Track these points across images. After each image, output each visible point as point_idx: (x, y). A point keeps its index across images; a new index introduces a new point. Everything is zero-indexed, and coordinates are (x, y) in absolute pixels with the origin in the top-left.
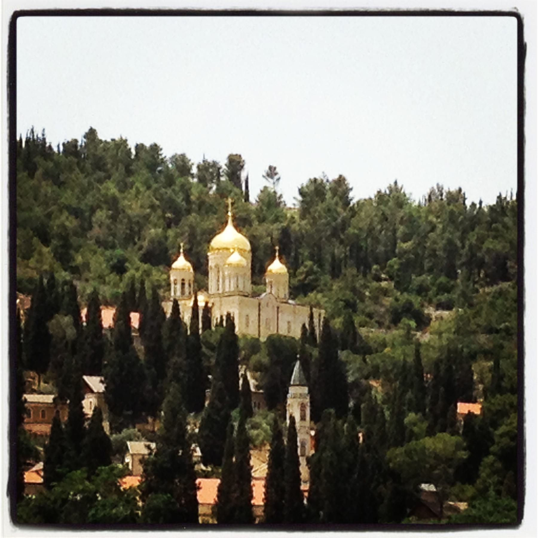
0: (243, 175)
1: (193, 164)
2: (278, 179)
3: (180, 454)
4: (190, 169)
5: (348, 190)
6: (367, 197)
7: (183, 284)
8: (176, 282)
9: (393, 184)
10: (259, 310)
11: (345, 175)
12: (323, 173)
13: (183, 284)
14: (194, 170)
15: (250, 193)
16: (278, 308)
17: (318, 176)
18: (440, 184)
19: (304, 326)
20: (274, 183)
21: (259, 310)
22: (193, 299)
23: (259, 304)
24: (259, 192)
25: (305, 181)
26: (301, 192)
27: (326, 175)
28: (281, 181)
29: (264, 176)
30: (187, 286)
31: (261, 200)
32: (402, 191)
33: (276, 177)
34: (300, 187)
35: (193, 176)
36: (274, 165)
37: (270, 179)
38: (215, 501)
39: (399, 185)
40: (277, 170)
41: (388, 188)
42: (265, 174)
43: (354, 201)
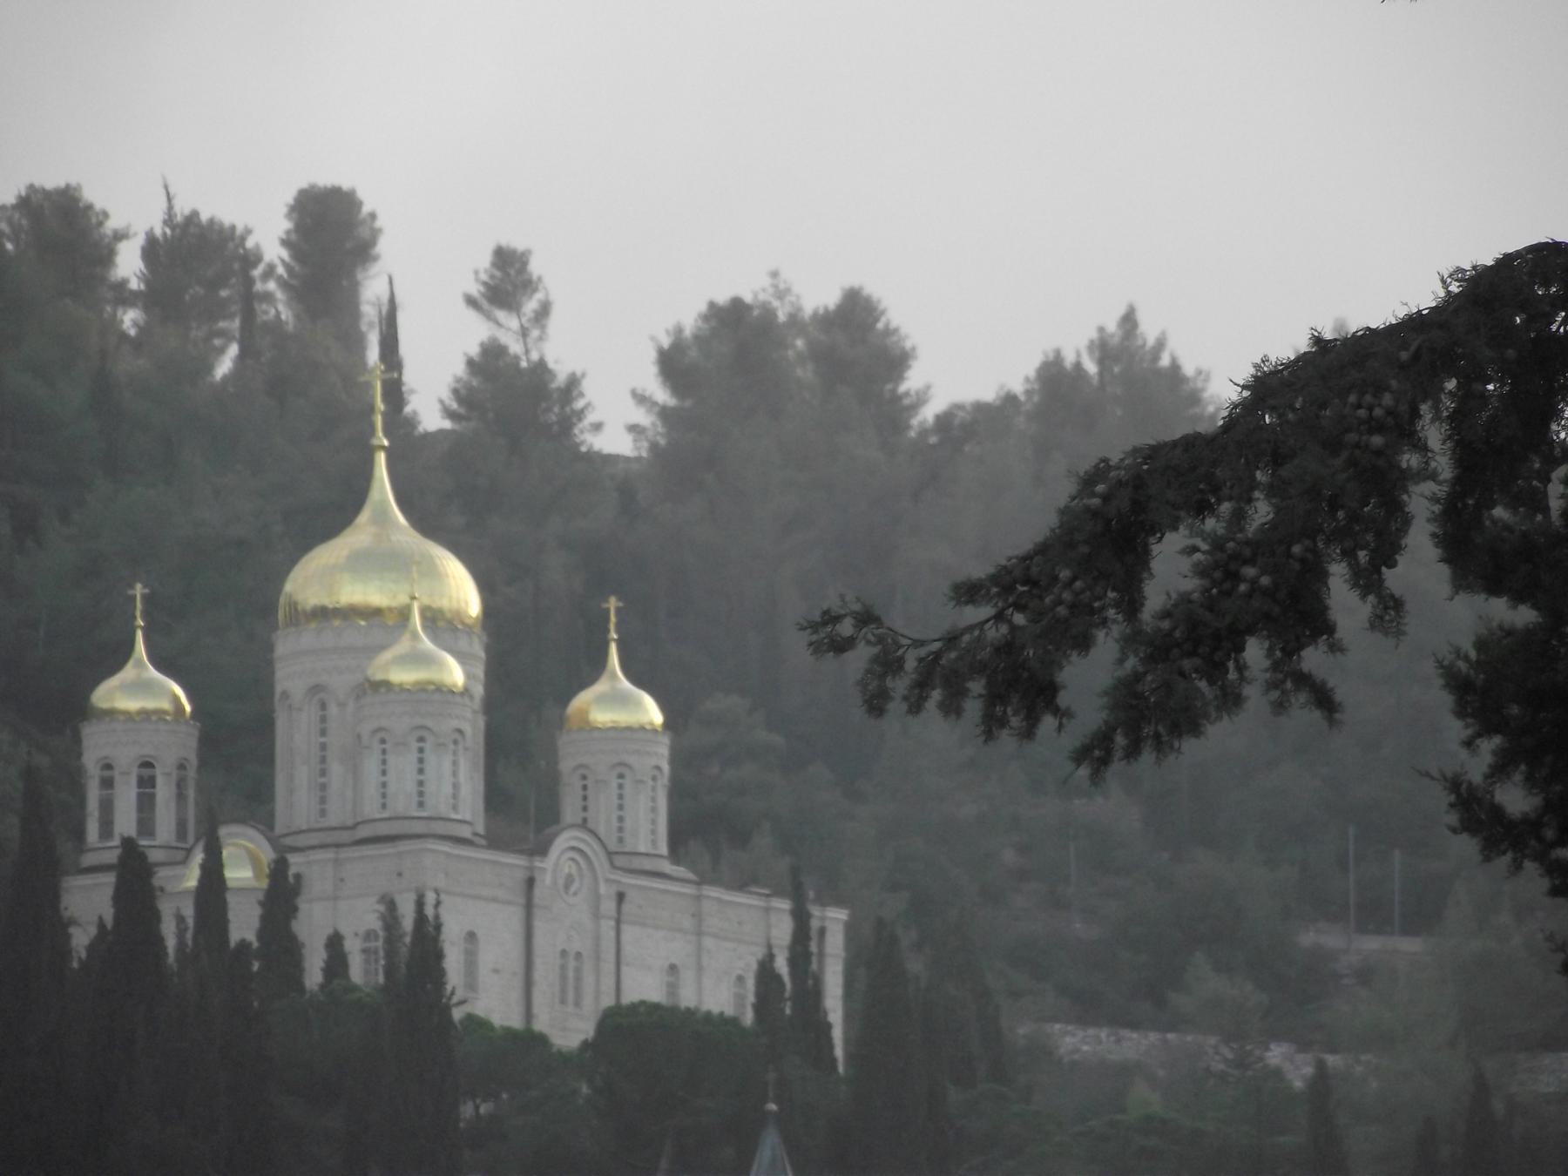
0: (372, 290)
1: (120, 236)
2: (544, 311)
3: (1518, 321)
4: (105, 255)
5: (895, 361)
6: (988, 394)
7: (147, 782)
8: (383, 690)
9: (1112, 326)
10: (529, 907)
11: (874, 288)
12: (775, 274)
13: (147, 782)
14: (129, 265)
15: (410, 377)
16: (621, 897)
17: (748, 286)
18: (933, 391)
19: (766, 971)
20: (524, 333)
21: (529, 907)
22: (198, 857)
23: (530, 883)
24: (460, 369)
25: (687, 314)
26: (672, 363)
27: (788, 291)
28: (555, 322)
29: (471, 302)
30: (164, 792)
31: (467, 401)
32: (1165, 361)
33: (531, 306)
34: (666, 342)
35: (122, 295)
36: (518, 243)
37: (501, 315)
38: (1407, 492)
39: (1149, 330)
40: (536, 267)
41: (1091, 347)
42: (475, 289)
43: (928, 413)
